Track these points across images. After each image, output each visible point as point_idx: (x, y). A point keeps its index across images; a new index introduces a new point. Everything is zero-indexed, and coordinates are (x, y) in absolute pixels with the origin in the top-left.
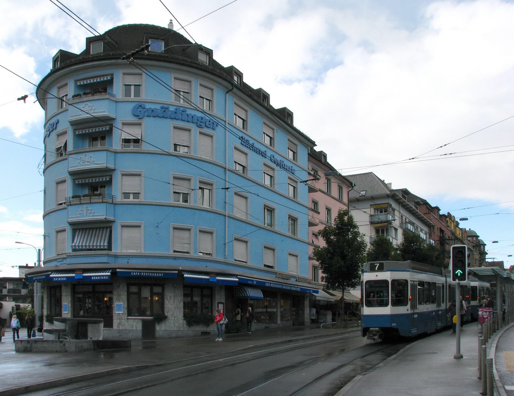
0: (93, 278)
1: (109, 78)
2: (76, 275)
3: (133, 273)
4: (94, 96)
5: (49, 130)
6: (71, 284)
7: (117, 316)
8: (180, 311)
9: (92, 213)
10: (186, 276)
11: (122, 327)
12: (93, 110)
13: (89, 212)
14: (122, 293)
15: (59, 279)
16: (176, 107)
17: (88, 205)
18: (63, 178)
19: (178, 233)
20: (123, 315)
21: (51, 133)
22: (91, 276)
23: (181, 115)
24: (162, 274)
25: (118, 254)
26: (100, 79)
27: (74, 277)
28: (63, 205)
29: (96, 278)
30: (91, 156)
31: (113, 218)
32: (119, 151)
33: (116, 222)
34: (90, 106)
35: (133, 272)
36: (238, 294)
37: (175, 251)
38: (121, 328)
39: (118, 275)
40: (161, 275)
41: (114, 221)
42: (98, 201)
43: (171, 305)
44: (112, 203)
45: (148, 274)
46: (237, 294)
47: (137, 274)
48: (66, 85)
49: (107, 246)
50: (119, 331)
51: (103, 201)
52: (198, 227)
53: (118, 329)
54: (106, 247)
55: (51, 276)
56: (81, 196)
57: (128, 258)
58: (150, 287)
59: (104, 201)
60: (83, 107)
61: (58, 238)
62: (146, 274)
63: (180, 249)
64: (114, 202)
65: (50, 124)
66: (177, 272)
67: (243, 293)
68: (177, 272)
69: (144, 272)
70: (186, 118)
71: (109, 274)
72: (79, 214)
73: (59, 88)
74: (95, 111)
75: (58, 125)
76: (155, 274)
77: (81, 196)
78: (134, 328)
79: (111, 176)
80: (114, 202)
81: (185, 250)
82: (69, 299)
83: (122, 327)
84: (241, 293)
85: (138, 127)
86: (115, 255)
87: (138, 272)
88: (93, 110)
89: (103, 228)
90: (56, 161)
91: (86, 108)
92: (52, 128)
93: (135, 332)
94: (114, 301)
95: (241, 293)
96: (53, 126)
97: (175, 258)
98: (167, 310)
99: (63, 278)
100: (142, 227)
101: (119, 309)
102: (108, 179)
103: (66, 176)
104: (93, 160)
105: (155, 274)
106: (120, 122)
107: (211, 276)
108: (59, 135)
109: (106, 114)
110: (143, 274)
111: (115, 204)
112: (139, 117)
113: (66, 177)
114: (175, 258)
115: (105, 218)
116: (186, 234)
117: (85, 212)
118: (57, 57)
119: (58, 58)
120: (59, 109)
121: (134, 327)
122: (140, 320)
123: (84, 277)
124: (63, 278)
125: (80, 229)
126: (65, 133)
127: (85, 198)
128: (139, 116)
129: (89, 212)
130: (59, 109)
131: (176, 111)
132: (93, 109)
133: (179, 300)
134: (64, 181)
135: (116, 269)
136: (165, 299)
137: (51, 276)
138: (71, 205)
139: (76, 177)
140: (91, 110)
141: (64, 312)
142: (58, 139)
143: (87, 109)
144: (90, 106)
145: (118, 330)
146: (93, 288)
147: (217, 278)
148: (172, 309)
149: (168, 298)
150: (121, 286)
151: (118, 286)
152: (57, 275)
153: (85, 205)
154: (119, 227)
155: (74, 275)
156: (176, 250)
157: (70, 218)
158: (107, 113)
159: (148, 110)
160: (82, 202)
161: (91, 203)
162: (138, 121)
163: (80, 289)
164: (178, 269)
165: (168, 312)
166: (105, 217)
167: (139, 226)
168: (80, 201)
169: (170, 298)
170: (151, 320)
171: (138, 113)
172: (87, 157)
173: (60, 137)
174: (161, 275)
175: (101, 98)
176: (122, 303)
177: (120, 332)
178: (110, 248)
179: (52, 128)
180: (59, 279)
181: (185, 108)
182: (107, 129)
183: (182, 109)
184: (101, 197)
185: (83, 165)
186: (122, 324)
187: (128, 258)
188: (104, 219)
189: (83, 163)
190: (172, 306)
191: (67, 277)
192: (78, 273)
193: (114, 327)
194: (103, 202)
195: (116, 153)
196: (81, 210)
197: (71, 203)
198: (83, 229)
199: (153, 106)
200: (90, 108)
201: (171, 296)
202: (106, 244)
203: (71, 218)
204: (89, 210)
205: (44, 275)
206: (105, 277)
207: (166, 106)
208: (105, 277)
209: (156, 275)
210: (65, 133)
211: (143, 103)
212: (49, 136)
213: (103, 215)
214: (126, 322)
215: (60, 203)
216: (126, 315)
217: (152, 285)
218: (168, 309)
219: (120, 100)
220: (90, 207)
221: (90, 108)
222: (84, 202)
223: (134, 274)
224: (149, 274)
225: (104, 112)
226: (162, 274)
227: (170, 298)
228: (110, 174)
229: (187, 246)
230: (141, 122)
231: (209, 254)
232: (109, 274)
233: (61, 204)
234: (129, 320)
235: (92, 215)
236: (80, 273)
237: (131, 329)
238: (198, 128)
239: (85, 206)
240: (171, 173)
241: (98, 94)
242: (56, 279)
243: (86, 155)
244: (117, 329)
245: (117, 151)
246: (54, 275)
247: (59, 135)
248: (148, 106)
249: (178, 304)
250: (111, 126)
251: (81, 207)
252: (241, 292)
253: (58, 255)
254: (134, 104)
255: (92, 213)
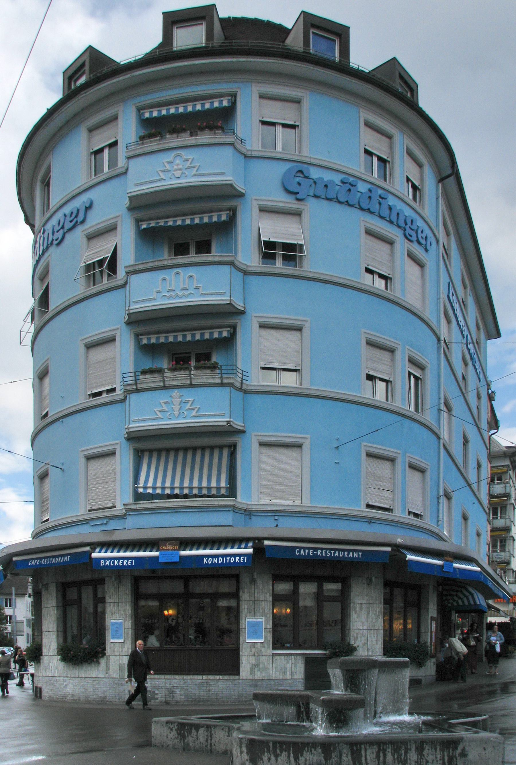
0: (205, 561)
1: (225, 103)
2: (161, 554)
3: (299, 552)
4: (197, 135)
5: (63, 228)
6: (131, 575)
7: (248, 650)
8: (377, 636)
9: (193, 409)
10: (410, 557)
11: (261, 673)
12: (195, 169)
13: (188, 406)
14: (262, 597)
15: (116, 563)
16: (369, 186)
17: (184, 391)
18: (111, 331)
19: (374, 464)
20: (264, 647)
21: (67, 236)
22: (203, 557)
23: (377, 206)
24: (360, 553)
25: (254, 508)
26: (203, 105)
27: (156, 558)
28: (104, 395)
29: (215, 561)
30: (191, 276)
31: (242, 425)
32: (253, 269)
33: (247, 434)
34: (186, 160)
35: (300, 548)
36: (454, 600)
37: (368, 506)
38: (258, 675)
39: (268, 555)
40: (359, 555)
41: (244, 432)
42: (211, 381)
43: (363, 623)
44: (240, 389)
45: (331, 553)
46: (451, 601)
47: (308, 553)
48: (115, 118)
49: (226, 488)
50: (255, 683)
51: (222, 381)
52: (407, 454)
53: (251, 677)
54: (223, 491)
55: (94, 555)
56: (164, 370)
57: (276, 518)
58: (316, 583)
59: (225, 381)
60: (169, 163)
61: (91, 473)
62: (326, 554)
63: (379, 502)
64: (244, 387)
65: (65, 215)
66: (389, 549)
67: (465, 599)
68: (389, 549)
69: (322, 549)
70: (385, 212)
71: (250, 551)
72: (160, 411)
73: (91, 130)
74: (199, 172)
75: (91, 214)
76: (346, 553)
77: (164, 370)
78: (288, 676)
79: (234, 328)
80: (244, 387)
81: (384, 503)
82: (125, 611)
83: (261, 673)
84: (460, 598)
85: (294, 219)
86: (245, 510)
87: (309, 549)
88: (195, 169)
89: (212, 448)
90: (42, 323)
91: (178, 165)
92: (71, 222)
93: (289, 684)
94: (244, 616)
95: (460, 598)
96: (76, 216)
97: (370, 521)
98: (355, 635)
99: (125, 562)
100: (306, 447)
101: (255, 633)
102: (225, 334)
103: (115, 327)
104: (195, 285)
105: (346, 553)
106: (255, 203)
107: (448, 561)
108: (91, 237)
109: (228, 178)
110: (321, 553)
111: (246, 392)
112: (298, 196)
113: (117, 329)
114: (370, 521)
115: (228, 422)
116: (385, 468)
117: (177, 407)
118: (78, 64)
119: (83, 65)
120: (90, 176)
121: (288, 673)
122: (299, 658)
123: (182, 557)
124: (125, 562)
125: (151, 451)
126: (112, 229)
127: (177, 373)
128: (298, 193)
129: (188, 406)
130: (90, 176)
131: (370, 194)
132: (194, 167)
133: (376, 611)
134: (111, 340)
135: (261, 539)
136: (351, 611)
137: (94, 555)
138: (138, 391)
139: (141, 329)
140: (189, 168)
141: (112, 641)
142: (88, 246)
143: (180, 167)
144: (186, 160)
145: (252, 680)
146: (186, 586)
147: (455, 565)
148: (365, 631)
149: (358, 606)
150: (259, 582)
151: (253, 581)
152: (109, 554)
153: (176, 391)
154: (255, 445)
155: (155, 553)
156: (370, 503)
157: (134, 421)
158: (230, 178)
159: (315, 183)
160: (168, 383)
161: (191, 386)
162: (294, 205)
163: (151, 588)
164: (393, 542)
165: (356, 639)
166: (228, 419)
167: (299, 446)
168: (164, 381)
169: (361, 609)
170: (322, 656)
171: (294, 188)
172: (181, 279)
173: (94, 242)
174: (359, 555)
175: (216, 141)
176: (262, 620)
177: (256, 686)
178: (232, 492)
179: (71, 222)
180: (116, 563)
181: (387, 193)
182: (224, 218)
183: (380, 192)
184: (218, 371)
185: (169, 298)
186: (261, 666)
187: (276, 518)
188: (225, 424)
189: (171, 293)
190: (363, 626)
191: (136, 559)
192: (168, 550)
193: (241, 674)
194: (222, 385)
195: (246, 273)
196: (166, 403)
197: (140, 386)
198: (159, 451)
199: (327, 176)
200: (188, 164)
201: (361, 604)
202: (223, 484)
203: (139, 421)
204: (187, 402)
205: (67, 555)
206: (238, 558)
207: (351, 179)
208: (238, 558)
209: (348, 555)
210: (112, 229)
211: (306, 166)
212: (58, 244)
213: (223, 415)
214: (271, 661)
215: (94, 392)
216: (271, 646)
217: (320, 580)
218: (357, 631)
219: (254, 154)
220: (189, 395)
221: (188, 164)
222: (175, 383)
223: (302, 552)
224: (334, 553)
225: (223, 174)
226: (360, 553)
227: (361, 609)
228: (231, 321)
229: (388, 494)
230: (303, 207)
231: (416, 515)
232: (250, 551)
233: (99, 394)
234: (276, 657)
235: (194, 413)
236: (173, 550)
237: (281, 677)
238: (406, 240)
239: (175, 393)
240: (363, 330)
241: (207, 131)
242: (108, 563)
243: (177, 273)
244: (249, 677)
245: (250, 269)
246: (102, 555)
247: (91, 237)
248: (315, 173)
249: (374, 621)
250: (233, 213)
251: (162, 397)
252: (462, 596)
253: (89, 511)
254: (285, 167)
255: (193, 409)
